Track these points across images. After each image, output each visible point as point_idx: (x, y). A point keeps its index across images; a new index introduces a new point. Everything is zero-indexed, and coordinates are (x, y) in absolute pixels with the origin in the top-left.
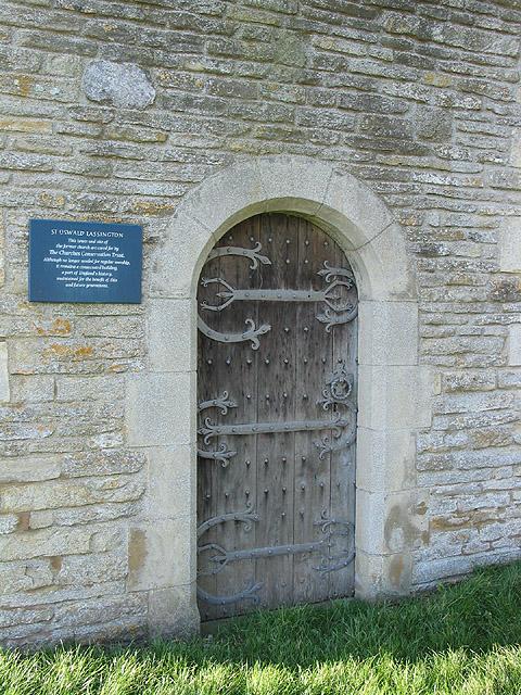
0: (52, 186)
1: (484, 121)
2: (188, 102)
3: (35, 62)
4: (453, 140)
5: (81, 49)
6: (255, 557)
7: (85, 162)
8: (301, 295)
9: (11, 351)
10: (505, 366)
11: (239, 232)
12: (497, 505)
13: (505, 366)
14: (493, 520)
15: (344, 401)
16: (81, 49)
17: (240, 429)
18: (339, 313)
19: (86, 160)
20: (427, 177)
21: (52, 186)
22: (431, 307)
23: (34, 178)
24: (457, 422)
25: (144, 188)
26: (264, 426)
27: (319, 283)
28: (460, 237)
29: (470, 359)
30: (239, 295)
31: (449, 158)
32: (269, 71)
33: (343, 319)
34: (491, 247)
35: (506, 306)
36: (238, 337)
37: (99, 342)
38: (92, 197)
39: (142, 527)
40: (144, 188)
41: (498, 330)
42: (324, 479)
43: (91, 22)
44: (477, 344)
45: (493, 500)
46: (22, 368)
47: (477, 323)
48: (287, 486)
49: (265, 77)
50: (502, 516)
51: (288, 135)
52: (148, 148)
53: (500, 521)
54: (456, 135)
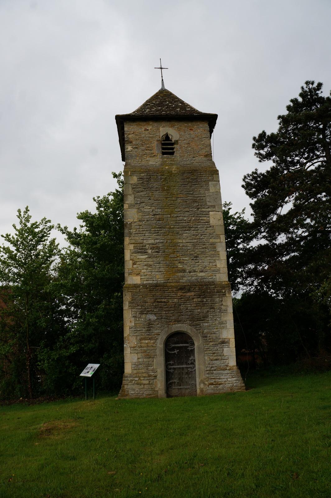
0: (142, 332)
1: (215, 313)
2: (162, 318)
3: (140, 316)
4: (209, 317)
5: (146, 314)
6: (178, 388)
7: (147, 329)
8: (184, 345)
9: (138, 355)
10: (223, 355)
11: (167, 343)
12: (224, 381)
13: (223, 355)
14: (223, 384)
15: (193, 363)
16: (146, 314)
17: (175, 367)
18: (191, 348)
19: (147, 328)
20: (205, 324)
21: (142, 332)
22: (206, 346)
23: (140, 332)
24: (213, 366)
25: (156, 331)
26: (179, 366)
27: (187, 343)
28: (211, 333)
29: (215, 354)
30: (173, 345)
31: (208, 321)
32: (174, 312)
33: (193, 348)
34: (218, 335)
35: (222, 345)
36: (174, 352)
37: (150, 353)
38: (148, 333)
39: (157, 381)
40: (156, 331)
41: (221, 349)
42: (190, 376)
43: (147, 310)
44: (217, 352)
45: (224, 380)
46: (139, 357)
47: (216, 348)
48: (183, 376)
49: (173, 313)
50: (225, 383)
51: (178, 321)
52: (156, 326)
53: (225, 384)
54: (210, 316)
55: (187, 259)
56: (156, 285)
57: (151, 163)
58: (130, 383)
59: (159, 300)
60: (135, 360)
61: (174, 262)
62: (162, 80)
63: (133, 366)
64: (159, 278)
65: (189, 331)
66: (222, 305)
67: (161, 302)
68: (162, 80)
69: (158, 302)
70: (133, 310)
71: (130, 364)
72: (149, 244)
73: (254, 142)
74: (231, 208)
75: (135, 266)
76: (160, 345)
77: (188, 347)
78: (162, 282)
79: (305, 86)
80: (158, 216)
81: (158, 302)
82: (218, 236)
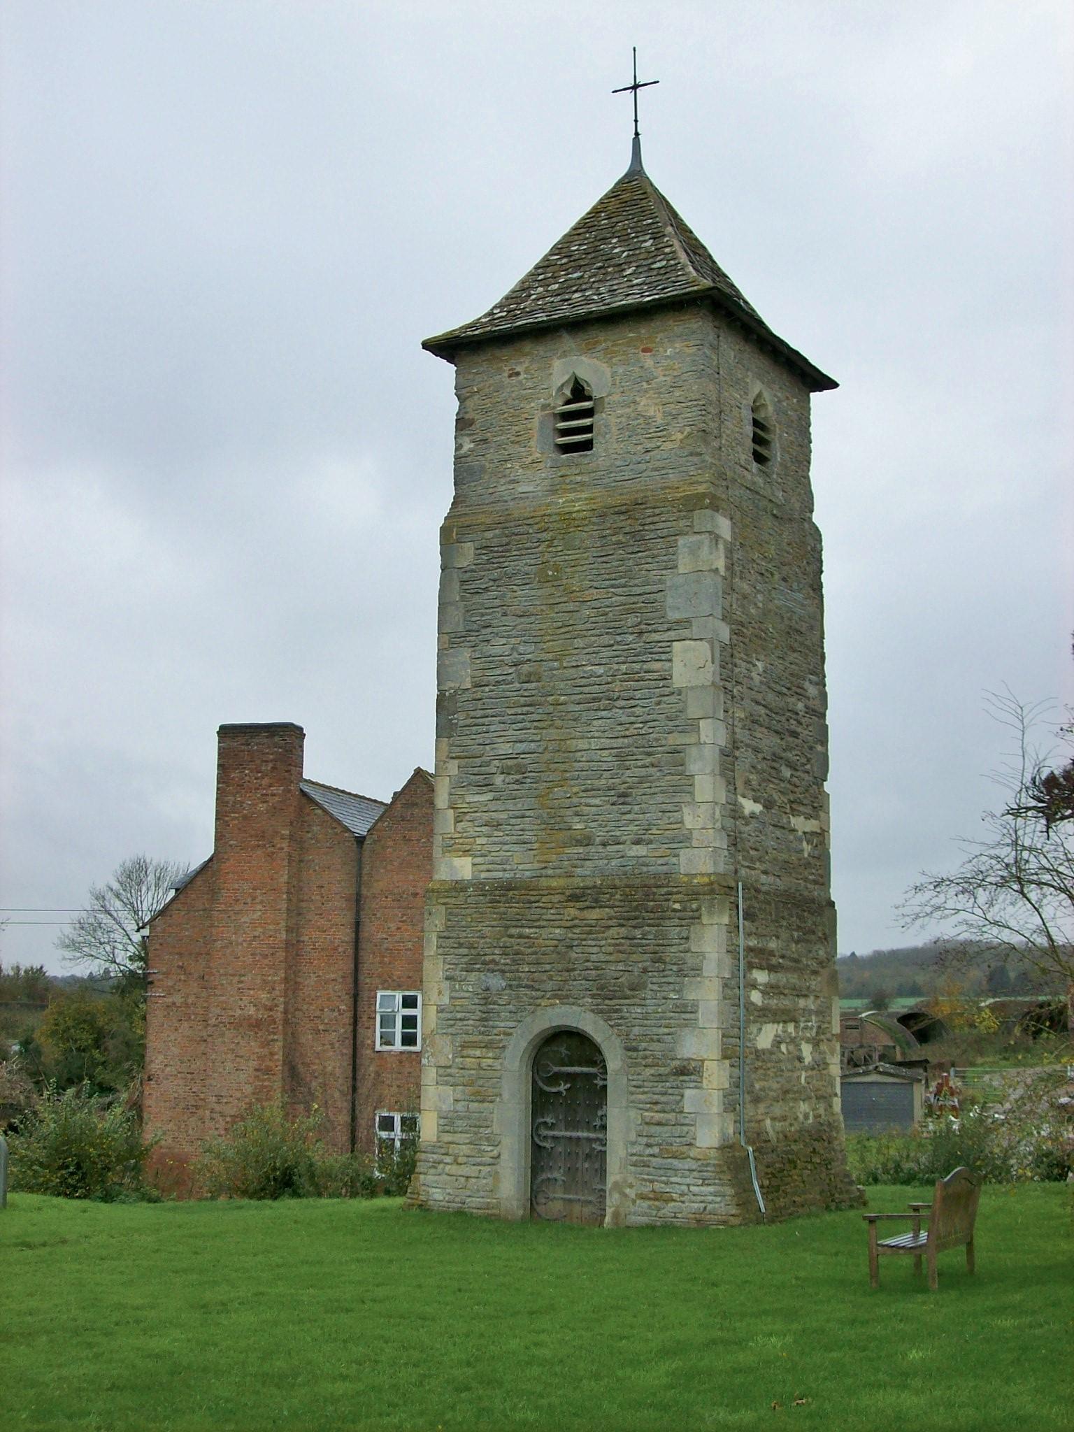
58: (432, 1171)
62: (637, 134)
63: (442, 1121)
67: (521, 936)
68: (637, 134)
71: (435, 1115)
77: (595, 1076)
81: (511, 936)
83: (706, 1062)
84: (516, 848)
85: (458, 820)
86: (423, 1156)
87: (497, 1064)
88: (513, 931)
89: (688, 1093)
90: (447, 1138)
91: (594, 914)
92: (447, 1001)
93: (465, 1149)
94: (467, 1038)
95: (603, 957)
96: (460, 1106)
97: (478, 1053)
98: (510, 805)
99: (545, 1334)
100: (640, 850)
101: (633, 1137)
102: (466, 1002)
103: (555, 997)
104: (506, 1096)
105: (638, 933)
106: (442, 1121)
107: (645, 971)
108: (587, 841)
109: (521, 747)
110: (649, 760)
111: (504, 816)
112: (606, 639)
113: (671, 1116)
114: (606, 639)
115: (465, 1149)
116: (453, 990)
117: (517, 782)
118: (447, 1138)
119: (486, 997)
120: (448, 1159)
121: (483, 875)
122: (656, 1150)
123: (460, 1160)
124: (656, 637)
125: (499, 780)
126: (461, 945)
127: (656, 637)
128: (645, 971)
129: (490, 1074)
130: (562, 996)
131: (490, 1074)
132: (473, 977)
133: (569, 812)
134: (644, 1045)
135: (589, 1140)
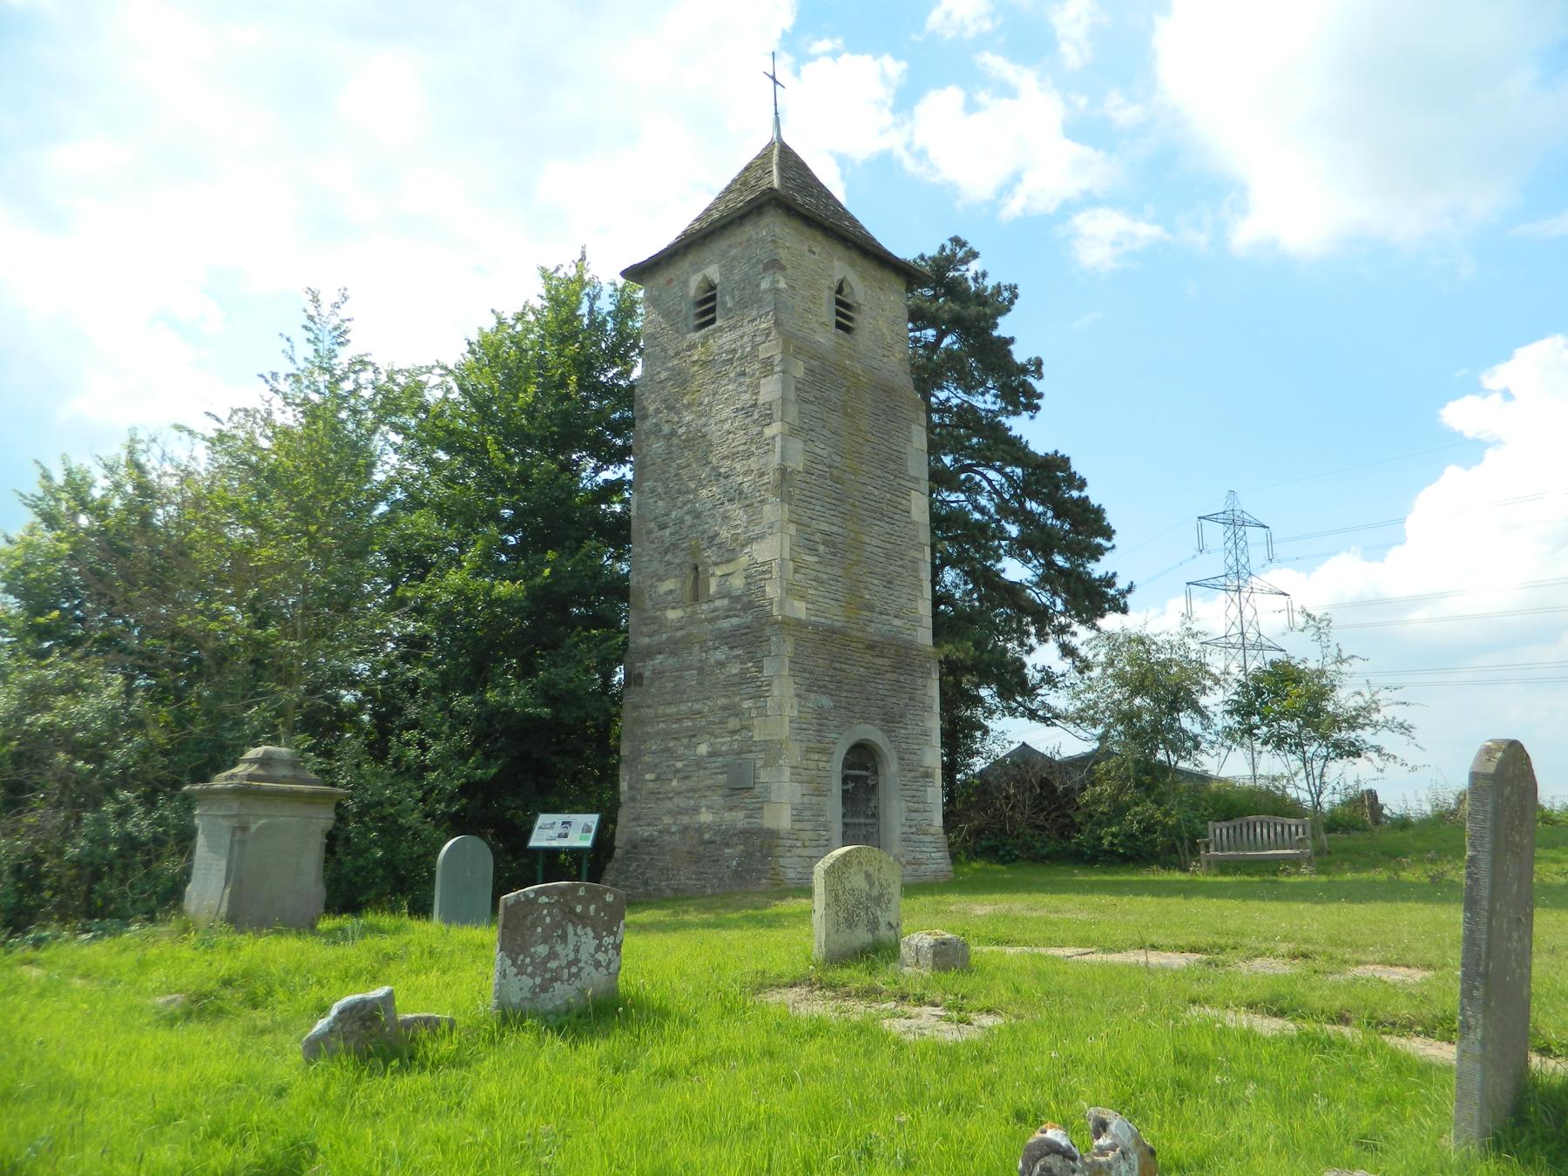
27: (866, 769)
55: (876, 582)
56: (833, 631)
57: (818, 338)
58: (788, 854)
59: (838, 665)
60: (798, 800)
61: (859, 584)
62: (776, 113)
63: (794, 812)
64: (835, 616)
65: (880, 743)
66: (214, 1086)
67: (841, 670)
68: (776, 113)
69: (835, 669)
70: (797, 680)
71: (789, 807)
72: (823, 532)
73: (1038, 385)
74: (1497, 443)
75: (798, 576)
76: (836, 766)
77: (866, 778)
78: (840, 624)
79: (949, 246)
80: (835, 472)
81: (835, 669)
82: (921, 546)
83: (1258, 772)
84: (832, 602)
85: (796, 571)
86: (781, 842)
87: (828, 766)
88: (838, 665)
89: (929, 789)
90: (798, 826)
91: (880, 661)
92: (796, 714)
93: (810, 834)
94: (811, 745)
95: (887, 693)
96: (806, 800)
97: (816, 757)
98: (829, 570)
99: (259, 1027)
100: (897, 622)
101: (904, 821)
102: (809, 716)
103: (862, 717)
104: (834, 790)
105: (902, 678)
106: (794, 812)
107: (907, 705)
108: (871, 608)
109: (834, 529)
110: (901, 563)
111: (825, 576)
112: (878, 472)
113: (921, 806)
114: (878, 472)
115: (810, 834)
116: (800, 705)
117: (831, 553)
118: (798, 826)
119: (821, 713)
120: (799, 844)
121: (813, 618)
122: (914, 830)
123: (807, 843)
124: (903, 482)
125: (821, 548)
126: (804, 671)
127: (903, 482)
128: (907, 705)
129: (824, 774)
130: (866, 719)
131: (824, 774)
132: (812, 696)
133: (862, 585)
134: (907, 756)
135: (865, 824)
